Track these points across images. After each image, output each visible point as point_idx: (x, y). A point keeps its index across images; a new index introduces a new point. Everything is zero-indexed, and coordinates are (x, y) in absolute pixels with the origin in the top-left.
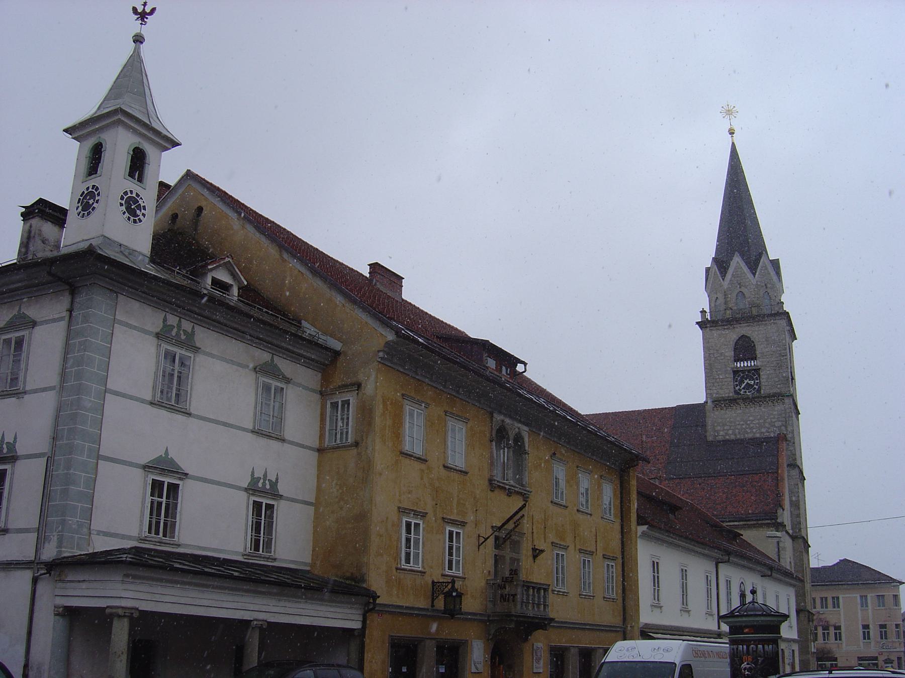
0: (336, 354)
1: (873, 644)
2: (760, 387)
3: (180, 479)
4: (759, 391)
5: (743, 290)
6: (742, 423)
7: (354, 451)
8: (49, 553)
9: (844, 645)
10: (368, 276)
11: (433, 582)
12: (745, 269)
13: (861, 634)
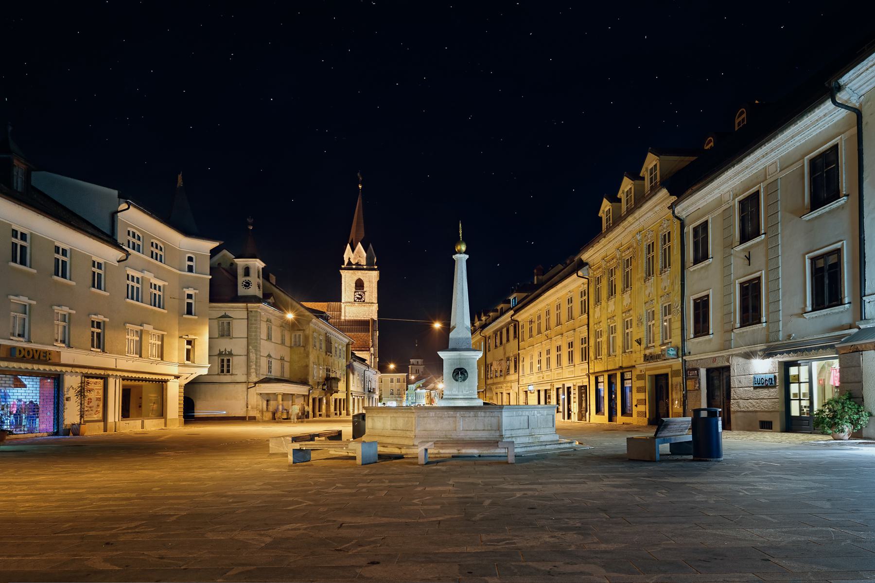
8: (254, 378)
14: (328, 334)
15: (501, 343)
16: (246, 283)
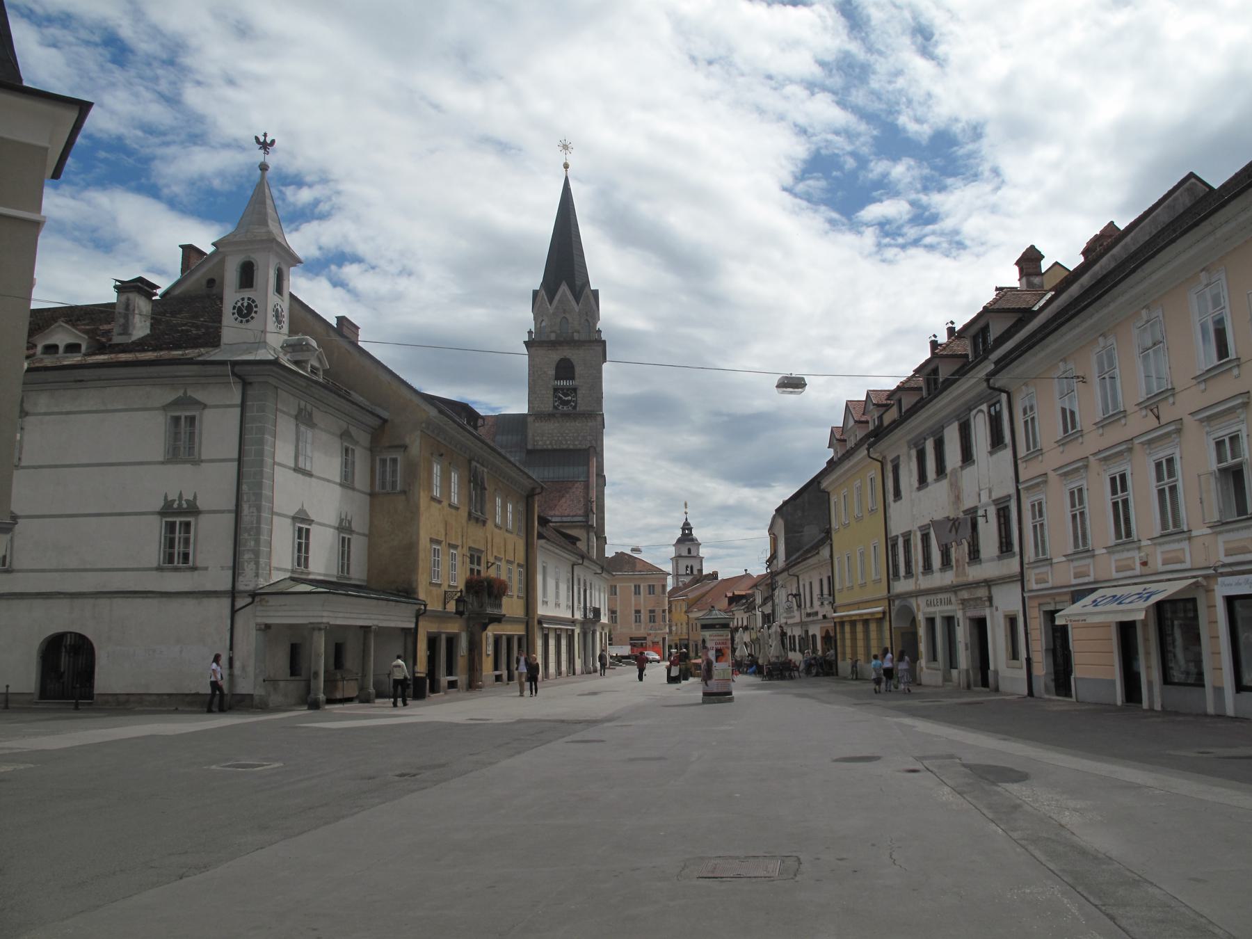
0: (385, 421)
1: (643, 626)
2: (576, 404)
3: (310, 525)
4: (575, 408)
5: (567, 316)
6: (559, 435)
7: (403, 497)
9: (619, 627)
10: (336, 326)
11: (445, 592)
12: (571, 297)
13: (633, 618)
14: (474, 463)
15: (941, 470)
16: (249, 308)
